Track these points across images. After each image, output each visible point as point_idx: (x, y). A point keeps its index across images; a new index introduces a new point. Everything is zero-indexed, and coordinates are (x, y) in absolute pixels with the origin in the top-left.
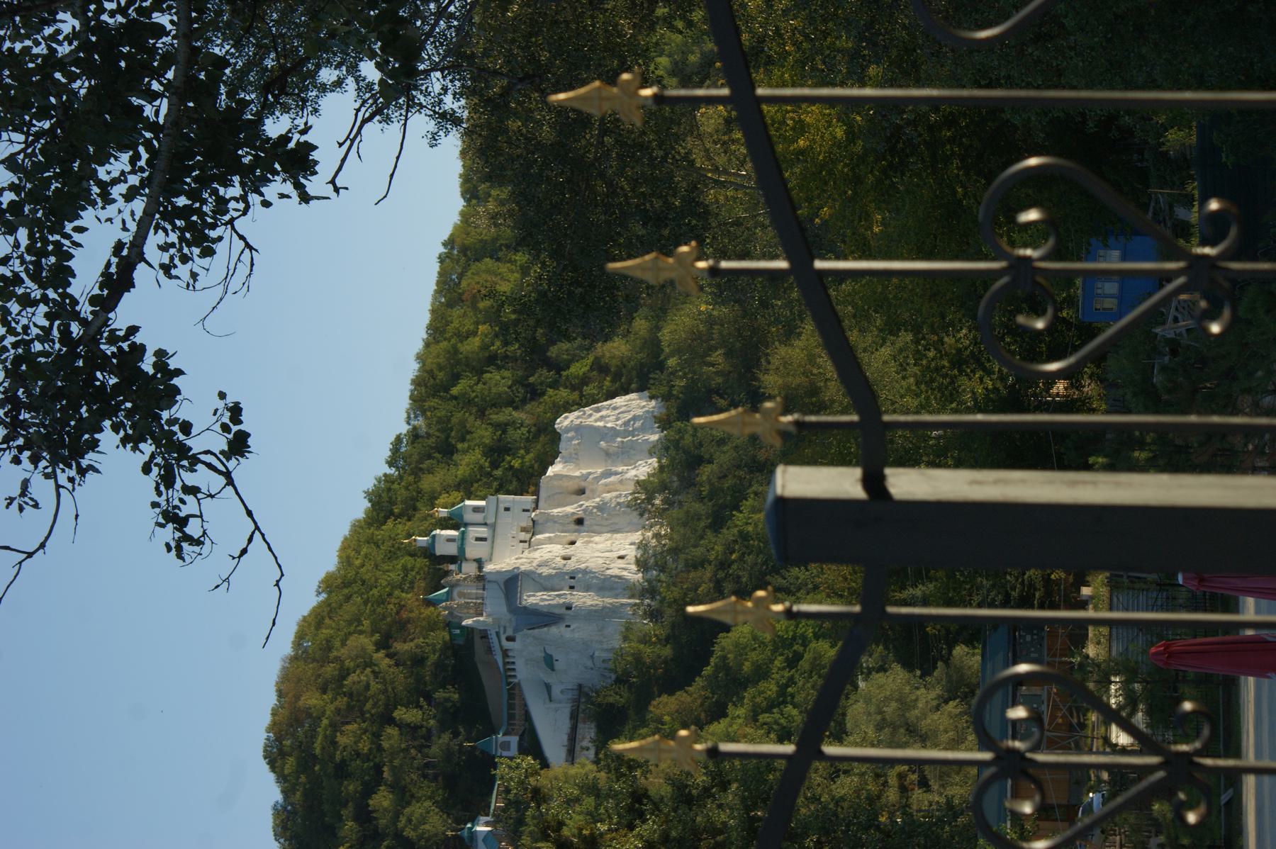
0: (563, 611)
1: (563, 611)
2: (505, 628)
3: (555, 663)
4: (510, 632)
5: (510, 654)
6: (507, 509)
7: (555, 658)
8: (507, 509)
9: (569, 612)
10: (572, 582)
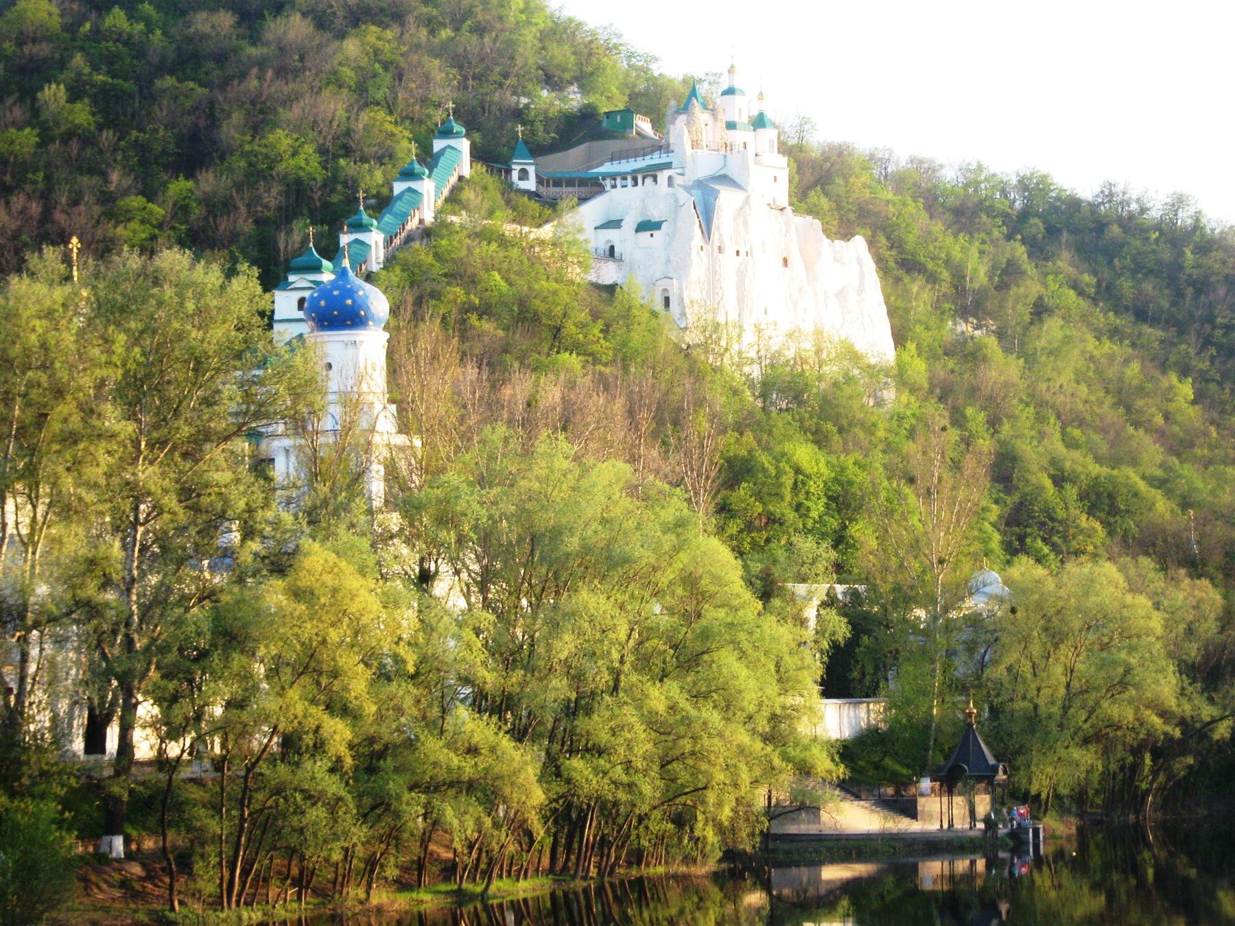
2: (682, 174)
3: (649, 233)
4: (678, 180)
5: (649, 181)
7: (655, 233)
9: (716, 250)
10: (742, 253)
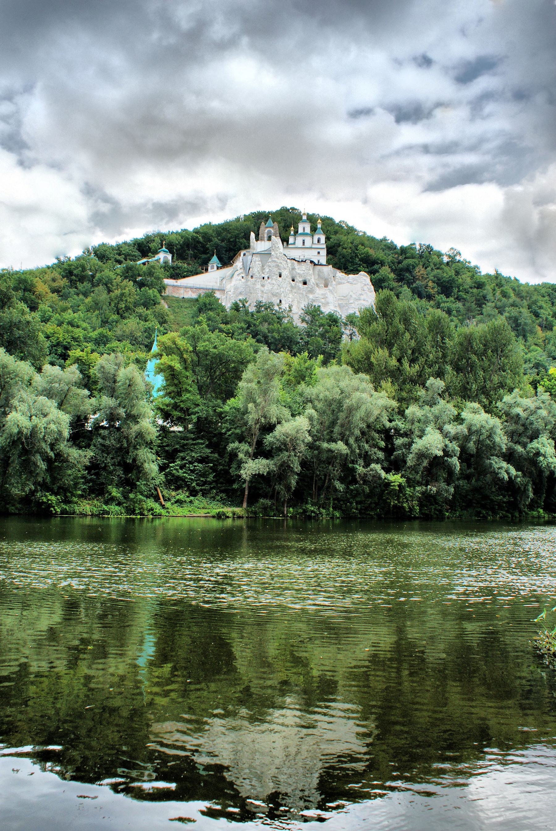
0: (251, 274)
1: (251, 274)
6: (319, 253)
8: (319, 253)
9: (250, 277)
10: (266, 278)
